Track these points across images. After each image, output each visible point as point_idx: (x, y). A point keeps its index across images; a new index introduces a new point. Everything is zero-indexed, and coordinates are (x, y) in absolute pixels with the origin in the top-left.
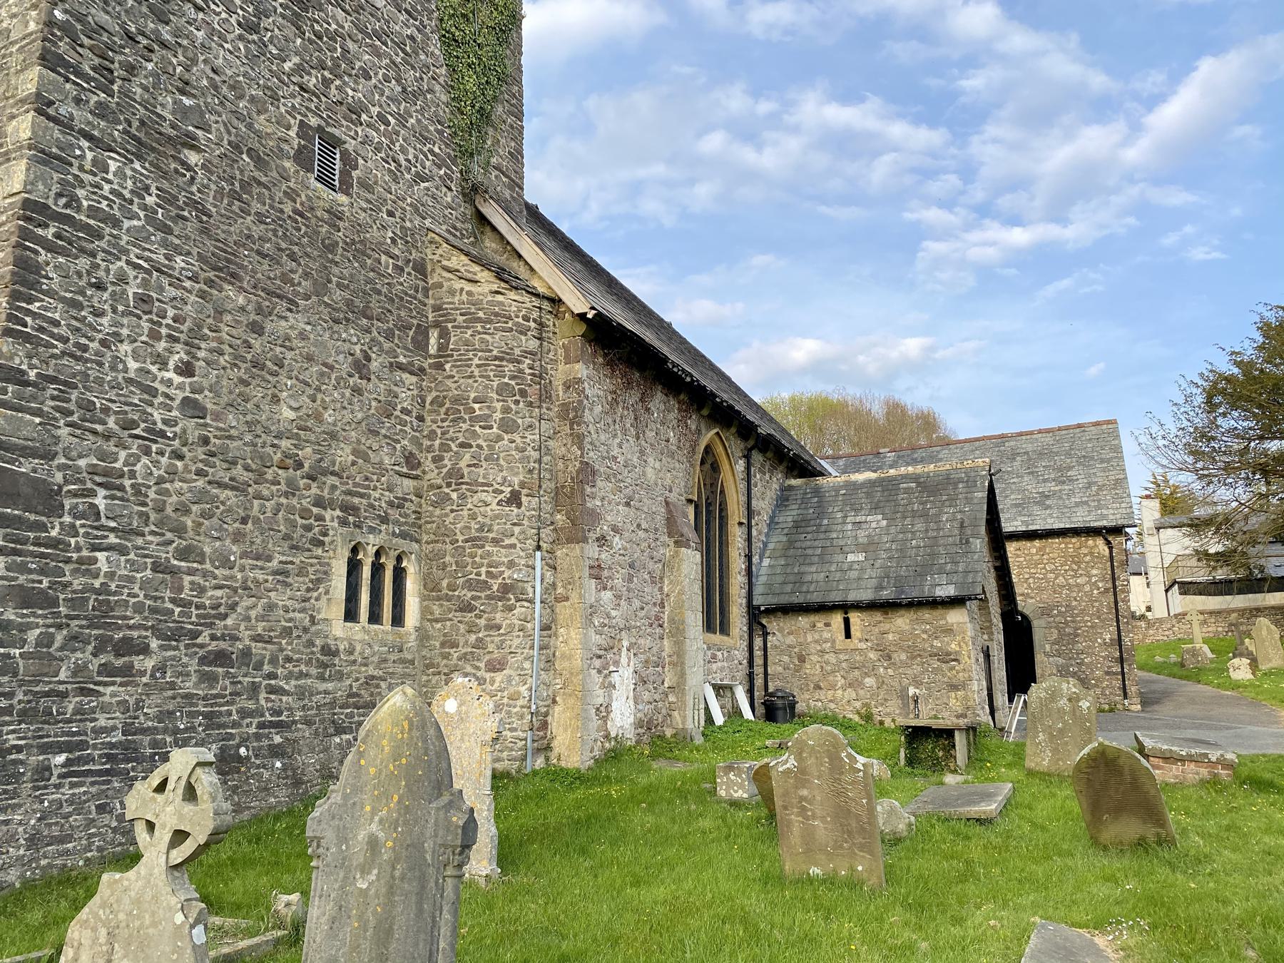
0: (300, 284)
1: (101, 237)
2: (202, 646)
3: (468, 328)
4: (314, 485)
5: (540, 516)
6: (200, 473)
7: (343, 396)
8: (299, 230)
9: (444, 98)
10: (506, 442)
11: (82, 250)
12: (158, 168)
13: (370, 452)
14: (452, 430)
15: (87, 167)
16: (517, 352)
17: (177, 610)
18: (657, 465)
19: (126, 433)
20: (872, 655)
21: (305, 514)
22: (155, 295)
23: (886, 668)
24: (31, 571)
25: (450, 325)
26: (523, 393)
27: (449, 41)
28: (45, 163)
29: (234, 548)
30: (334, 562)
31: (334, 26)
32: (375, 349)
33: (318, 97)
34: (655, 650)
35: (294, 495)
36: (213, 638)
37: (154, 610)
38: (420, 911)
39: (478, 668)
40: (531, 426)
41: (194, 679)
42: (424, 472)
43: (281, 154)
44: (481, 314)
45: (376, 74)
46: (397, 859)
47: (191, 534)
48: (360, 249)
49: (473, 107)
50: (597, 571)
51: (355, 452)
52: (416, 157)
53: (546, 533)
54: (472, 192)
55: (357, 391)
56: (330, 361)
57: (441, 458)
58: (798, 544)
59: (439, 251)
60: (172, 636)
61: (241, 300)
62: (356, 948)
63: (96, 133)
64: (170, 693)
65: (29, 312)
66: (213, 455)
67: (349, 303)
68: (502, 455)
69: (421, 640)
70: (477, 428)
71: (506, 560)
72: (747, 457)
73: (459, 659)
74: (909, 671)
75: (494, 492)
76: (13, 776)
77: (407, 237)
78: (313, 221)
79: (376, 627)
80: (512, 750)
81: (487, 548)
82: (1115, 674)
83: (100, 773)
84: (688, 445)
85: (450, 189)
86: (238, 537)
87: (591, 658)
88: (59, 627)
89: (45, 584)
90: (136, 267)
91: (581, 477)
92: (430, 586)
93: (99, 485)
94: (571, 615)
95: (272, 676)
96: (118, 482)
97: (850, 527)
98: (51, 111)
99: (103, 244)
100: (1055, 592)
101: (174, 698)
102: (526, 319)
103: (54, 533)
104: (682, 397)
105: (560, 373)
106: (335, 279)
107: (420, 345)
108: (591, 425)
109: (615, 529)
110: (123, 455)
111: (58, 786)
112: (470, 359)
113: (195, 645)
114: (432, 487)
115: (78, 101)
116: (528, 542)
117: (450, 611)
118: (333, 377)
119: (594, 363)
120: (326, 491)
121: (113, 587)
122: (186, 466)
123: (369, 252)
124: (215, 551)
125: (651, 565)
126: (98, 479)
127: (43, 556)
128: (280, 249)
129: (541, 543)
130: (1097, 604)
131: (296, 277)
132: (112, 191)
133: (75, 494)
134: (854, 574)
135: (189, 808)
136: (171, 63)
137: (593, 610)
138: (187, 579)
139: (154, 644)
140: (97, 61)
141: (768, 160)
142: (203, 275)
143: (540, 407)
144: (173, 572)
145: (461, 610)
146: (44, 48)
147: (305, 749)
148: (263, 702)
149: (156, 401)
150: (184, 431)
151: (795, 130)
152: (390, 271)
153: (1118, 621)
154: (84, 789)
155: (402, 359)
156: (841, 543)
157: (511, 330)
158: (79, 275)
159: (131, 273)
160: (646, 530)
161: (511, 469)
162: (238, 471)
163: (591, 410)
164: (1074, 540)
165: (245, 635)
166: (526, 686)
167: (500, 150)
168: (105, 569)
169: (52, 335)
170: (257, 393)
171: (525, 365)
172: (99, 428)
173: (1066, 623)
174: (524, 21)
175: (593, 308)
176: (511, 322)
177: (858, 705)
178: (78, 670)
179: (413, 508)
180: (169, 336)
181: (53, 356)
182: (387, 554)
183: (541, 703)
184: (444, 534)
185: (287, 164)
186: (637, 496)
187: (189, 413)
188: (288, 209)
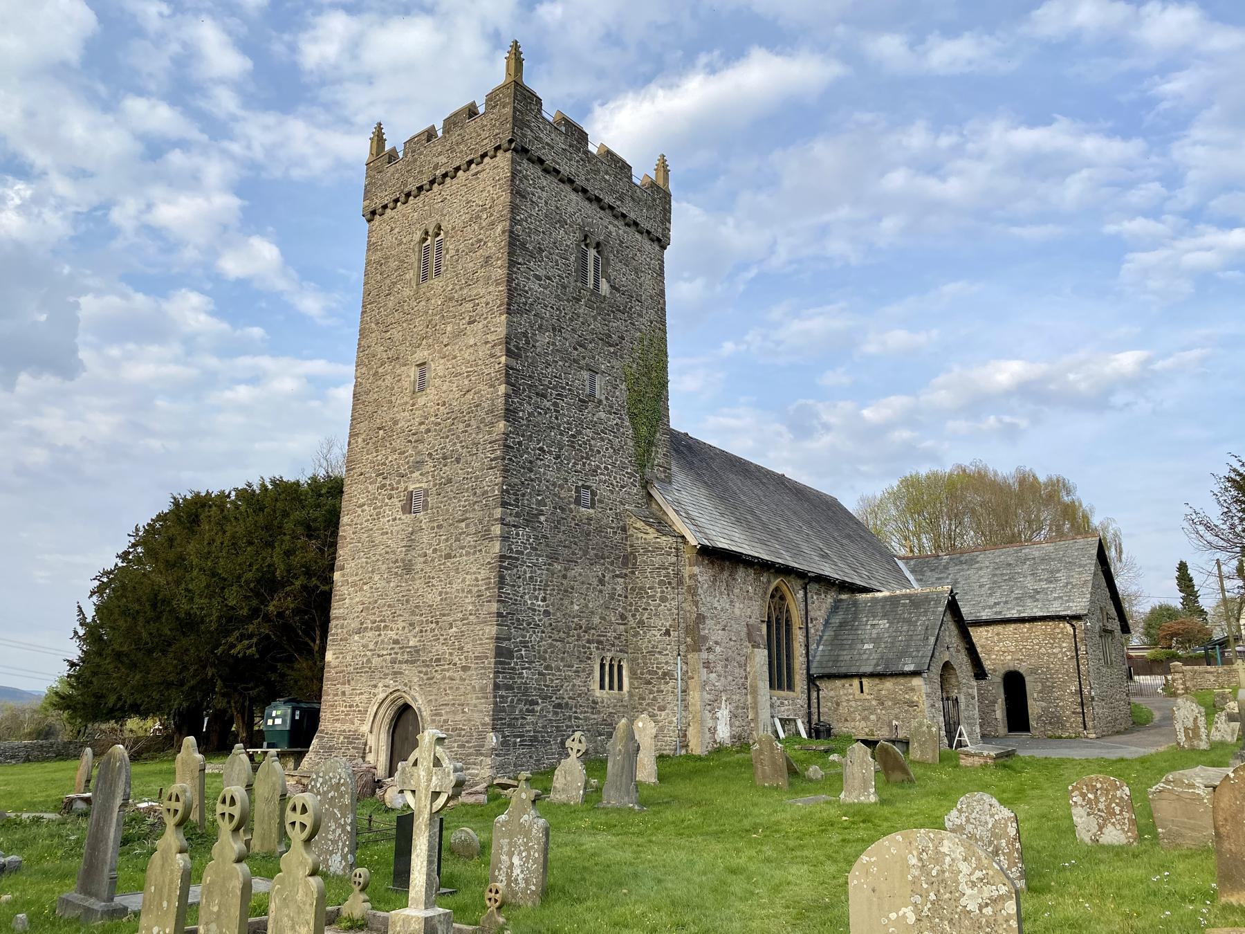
6: (550, 637)
16: (667, 564)
18: (741, 606)
20: (874, 703)
21: (584, 647)
23: (881, 710)
26: (670, 583)
27: (633, 417)
30: (595, 666)
34: (742, 701)
36: (557, 698)
37: (539, 689)
43: (570, 503)
44: (650, 548)
48: (599, 530)
50: (707, 665)
51: (600, 618)
52: (620, 478)
53: (683, 647)
54: (646, 484)
55: (601, 591)
58: (840, 637)
61: (559, 567)
65: (503, 593)
72: (805, 589)
74: (893, 712)
82: (1079, 713)
83: (529, 745)
84: (761, 591)
86: (562, 660)
88: (515, 696)
95: (576, 712)
97: (869, 627)
99: (519, 562)
100: (1039, 658)
102: (670, 548)
105: (687, 571)
109: (717, 643)
114: (631, 628)
125: (738, 658)
130: (1066, 667)
131: (576, 551)
133: (516, 651)
134: (865, 657)
137: (706, 683)
139: (540, 701)
140: (514, 497)
141: (952, 188)
144: (544, 675)
151: (980, 156)
153: (1079, 678)
155: (618, 573)
156: (863, 637)
160: (735, 641)
161: (665, 619)
163: (702, 588)
164: (1050, 624)
165: (566, 696)
170: (566, 602)
173: (1047, 678)
177: (867, 730)
184: (638, 649)
185: (572, 506)
188: (573, 525)
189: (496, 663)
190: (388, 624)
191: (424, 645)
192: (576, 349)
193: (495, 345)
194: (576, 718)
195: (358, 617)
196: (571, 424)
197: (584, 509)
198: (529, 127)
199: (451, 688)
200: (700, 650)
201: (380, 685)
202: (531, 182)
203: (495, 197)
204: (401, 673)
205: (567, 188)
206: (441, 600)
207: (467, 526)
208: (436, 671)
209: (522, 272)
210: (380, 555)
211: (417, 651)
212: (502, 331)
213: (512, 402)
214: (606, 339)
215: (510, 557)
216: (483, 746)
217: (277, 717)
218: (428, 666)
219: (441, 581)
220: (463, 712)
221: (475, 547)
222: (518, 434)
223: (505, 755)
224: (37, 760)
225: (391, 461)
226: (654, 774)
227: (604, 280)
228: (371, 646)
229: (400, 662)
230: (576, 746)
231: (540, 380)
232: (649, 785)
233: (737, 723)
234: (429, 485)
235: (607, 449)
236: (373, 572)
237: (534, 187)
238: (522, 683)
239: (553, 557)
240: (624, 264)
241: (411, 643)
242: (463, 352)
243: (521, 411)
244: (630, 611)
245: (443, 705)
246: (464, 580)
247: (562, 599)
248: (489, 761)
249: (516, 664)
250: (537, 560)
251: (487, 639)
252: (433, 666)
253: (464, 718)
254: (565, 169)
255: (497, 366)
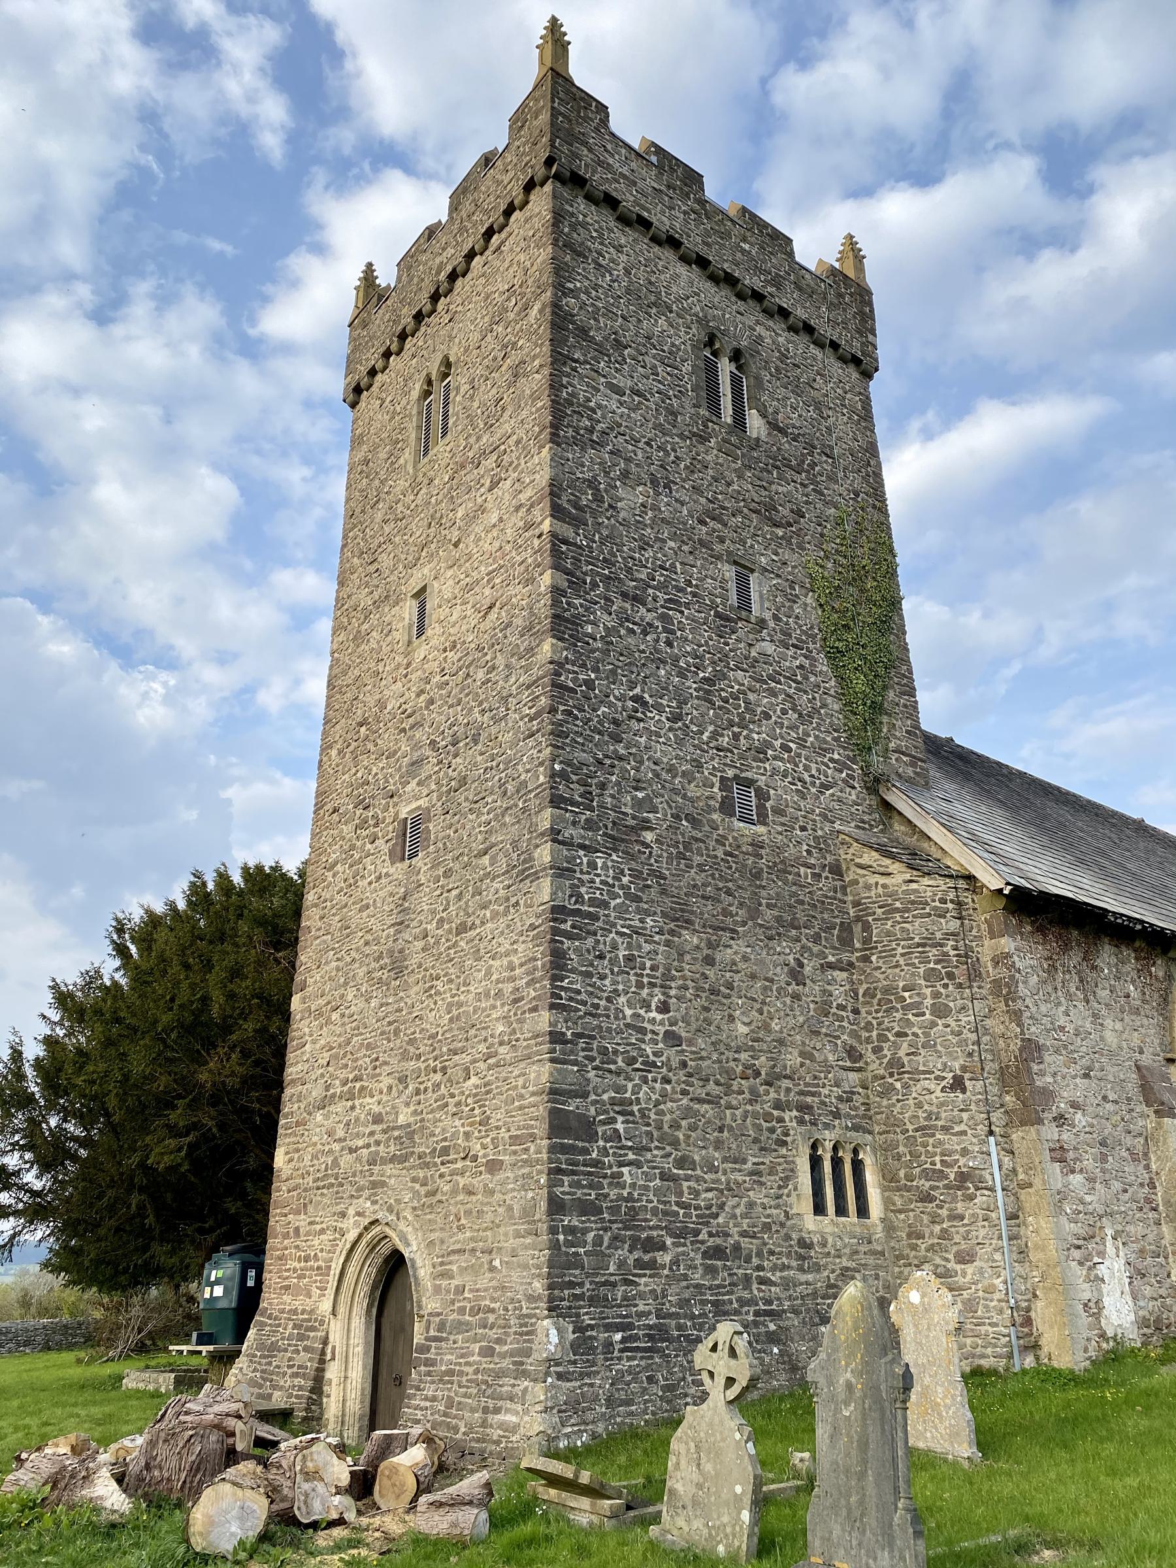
0: (737, 914)
1: (598, 919)
2: (702, 1242)
3: (887, 919)
4: (772, 1090)
5: (987, 1099)
6: (684, 1093)
7: (784, 1004)
8: (730, 868)
9: (836, 707)
10: (940, 1027)
11: (588, 932)
12: (627, 853)
13: (815, 1052)
14: (886, 1020)
15: (585, 870)
16: (939, 935)
17: (682, 1212)
18: (1118, 1026)
19: (630, 1068)
21: (768, 1117)
22: (636, 953)
24: (584, 1187)
25: (870, 919)
26: (951, 976)
27: (834, 655)
28: (560, 876)
29: (717, 1155)
30: (798, 1160)
31: (737, 687)
32: (806, 955)
33: (732, 752)
34: (1151, 1238)
35: (756, 1101)
36: (711, 1235)
37: (666, 1213)
38: (883, 1430)
39: (947, 1260)
40: (963, 1008)
41: (700, 1271)
42: (867, 1063)
43: (710, 810)
44: (898, 905)
45: (775, 712)
46: (865, 1396)
47: (683, 1145)
48: (782, 869)
49: (865, 704)
50: (1059, 1154)
51: (802, 1054)
52: (818, 770)
53: (997, 1116)
54: (874, 784)
55: (796, 997)
56: (770, 974)
57: (881, 1049)
59: (851, 851)
60: (680, 1234)
61: (695, 941)
62: (848, 1455)
63: (587, 843)
64: (684, 1283)
65: (562, 988)
66: (690, 1075)
67: (778, 919)
68: (938, 1041)
69: (888, 1232)
70: (910, 1016)
71: (958, 1148)
73: (927, 1250)
75: (936, 1079)
76: (590, 1349)
77: (821, 845)
78: (741, 856)
79: (843, 1219)
80: (996, 1346)
81: (938, 1136)
84: (1156, 996)
85: (854, 788)
86: (718, 1144)
87: (1069, 1249)
88: (605, 1229)
89: (593, 1196)
90: (622, 934)
91: (1024, 1056)
92: (889, 1177)
93: (618, 1113)
94: (1037, 1202)
95: (760, 1268)
96: (629, 1108)
98: (560, 838)
99: (600, 924)
101: (688, 1288)
103: (594, 1155)
104: (1137, 944)
105: (986, 950)
106: (764, 902)
107: (846, 942)
108: (1027, 1000)
109: (1075, 1105)
110: (630, 1086)
111: (619, 1359)
112: (894, 949)
113: (698, 1241)
115: (574, 823)
116: (978, 1128)
117: (911, 1201)
118: (774, 988)
119: (1022, 934)
120: (782, 1094)
121: (636, 1196)
122: (673, 1088)
123: (789, 869)
124: (703, 1158)
125: (1128, 1141)
126: (617, 1108)
127: (590, 1174)
128: (719, 889)
129: (993, 1128)
132: (602, 882)
133: (603, 1123)
135: (733, 1362)
136: (627, 770)
137: (1062, 1196)
138: (685, 1184)
139: (669, 1241)
140: (582, 789)
142: (666, 927)
143: (970, 987)
144: (675, 1179)
145: (922, 1201)
146: (552, 794)
147: (797, 1338)
148: (756, 1292)
149: (647, 1038)
150: (669, 1059)
152: (809, 881)
154: (636, 1362)
155: (831, 959)
157: (929, 915)
158: (588, 951)
159: (619, 940)
160: (1115, 1102)
162: (711, 1086)
163: (1025, 982)
166: (1000, 1279)
167: (897, 733)
168: (629, 1181)
169: (577, 1002)
170: (716, 1016)
171: (949, 947)
172: (612, 1067)
174: (903, 602)
175: (1008, 884)
176: (928, 908)
178: (621, 1264)
179: (861, 1100)
180: (650, 983)
181: (580, 1017)
182: (843, 1148)
183: (1020, 1297)
184: (893, 1124)
185: (715, 816)
186: (1097, 1065)
187: (671, 1043)
188: (720, 853)
189: (552, 1149)
190: (366, 1084)
191: (422, 1120)
192: (702, 522)
193: (532, 506)
194: (763, 1281)
195: (322, 1075)
196: (702, 658)
197: (742, 824)
198: (585, 144)
199: (468, 1213)
200: (1040, 1121)
201: (351, 1211)
202: (595, 234)
203: (528, 264)
204: (383, 1184)
205: (668, 254)
206: (451, 1020)
207: (493, 861)
208: (441, 1176)
209: (581, 377)
210: (357, 950)
211: (411, 1135)
212: (543, 477)
213: (568, 604)
214: (767, 512)
215: (577, 912)
216: (528, 1353)
217: (218, 1282)
218: (427, 1165)
219: (451, 981)
220: (492, 1269)
221: (507, 899)
222: (584, 666)
223: (582, 1376)
224: (60, 1348)
225: (376, 774)
226: (967, 1433)
227: (754, 411)
228: (340, 1133)
229: (384, 1161)
230: (722, 1365)
231: (629, 570)
232: (955, 1464)
233: (1148, 1291)
234: (431, 800)
235: (784, 712)
236: (346, 984)
237: (601, 244)
238: (620, 1198)
239: (680, 918)
240: (793, 391)
241: (402, 1119)
242: (481, 543)
243: (589, 622)
244: (868, 1040)
245: (454, 1252)
246: (488, 973)
247: (706, 1009)
248: (538, 1392)
249: (604, 1152)
250: (642, 921)
251: (533, 1094)
252: (435, 1164)
253: (494, 1284)
254: (661, 220)
255: (536, 542)
